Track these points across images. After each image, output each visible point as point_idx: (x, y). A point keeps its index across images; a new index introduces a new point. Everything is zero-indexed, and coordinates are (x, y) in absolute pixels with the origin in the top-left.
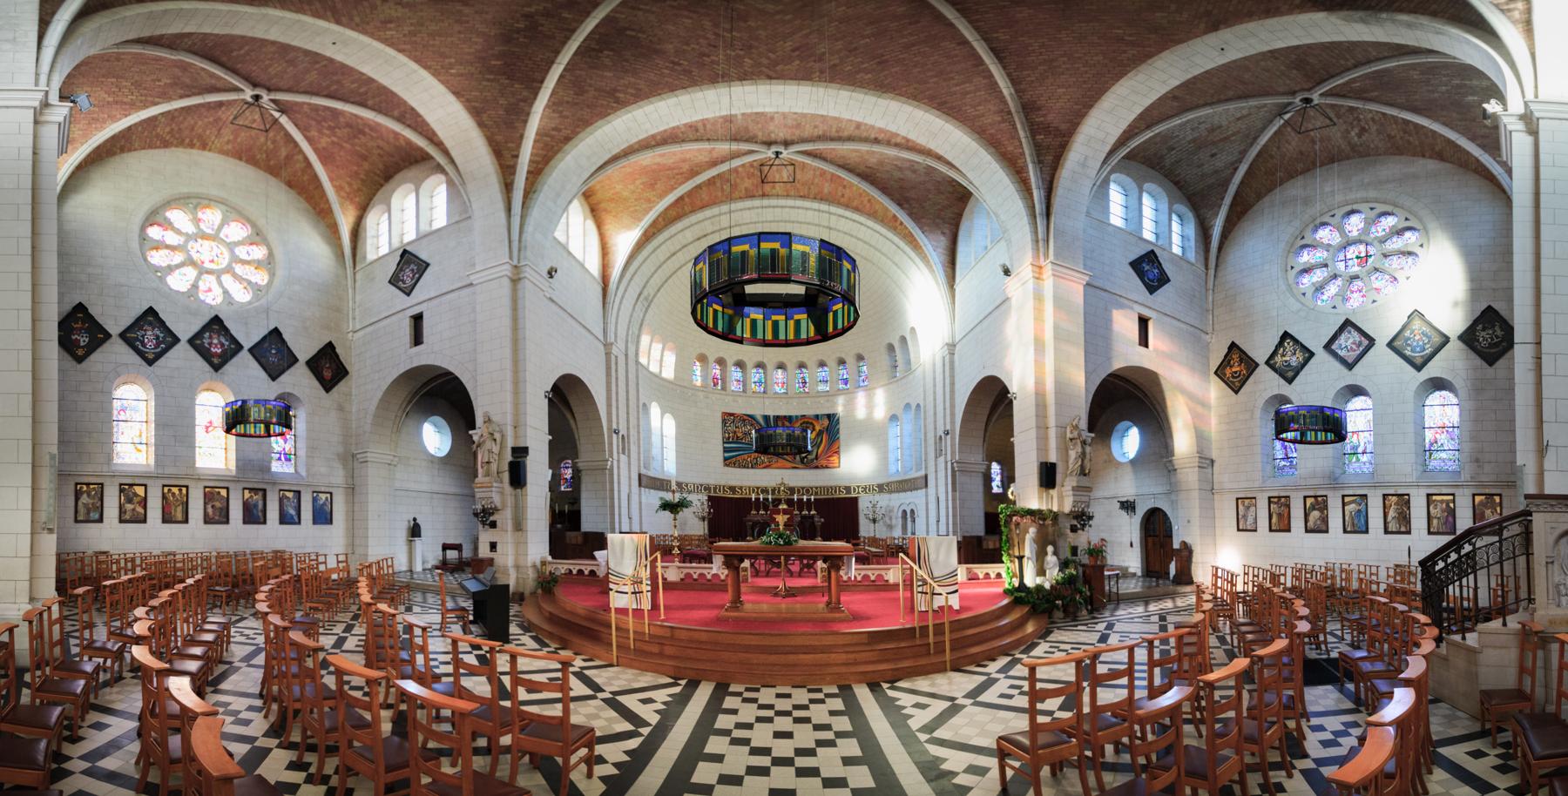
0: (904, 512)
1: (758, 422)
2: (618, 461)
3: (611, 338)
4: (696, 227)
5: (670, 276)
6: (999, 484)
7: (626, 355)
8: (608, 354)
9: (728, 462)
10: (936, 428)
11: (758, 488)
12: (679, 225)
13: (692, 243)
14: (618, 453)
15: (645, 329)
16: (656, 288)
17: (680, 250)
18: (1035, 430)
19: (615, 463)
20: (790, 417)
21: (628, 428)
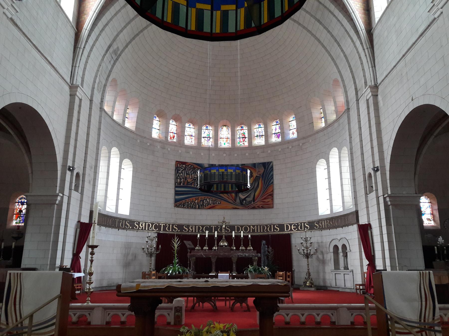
0: (336, 247)
2: (69, 197)
3: (78, 81)
6: (430, 217)
7: (91, 101)
8: (72, 96)
9: (178, 203)
10: (364, 167)
11: (203, 226)
14: (70, 189)
19: (65, 199)
21: (84, 168)
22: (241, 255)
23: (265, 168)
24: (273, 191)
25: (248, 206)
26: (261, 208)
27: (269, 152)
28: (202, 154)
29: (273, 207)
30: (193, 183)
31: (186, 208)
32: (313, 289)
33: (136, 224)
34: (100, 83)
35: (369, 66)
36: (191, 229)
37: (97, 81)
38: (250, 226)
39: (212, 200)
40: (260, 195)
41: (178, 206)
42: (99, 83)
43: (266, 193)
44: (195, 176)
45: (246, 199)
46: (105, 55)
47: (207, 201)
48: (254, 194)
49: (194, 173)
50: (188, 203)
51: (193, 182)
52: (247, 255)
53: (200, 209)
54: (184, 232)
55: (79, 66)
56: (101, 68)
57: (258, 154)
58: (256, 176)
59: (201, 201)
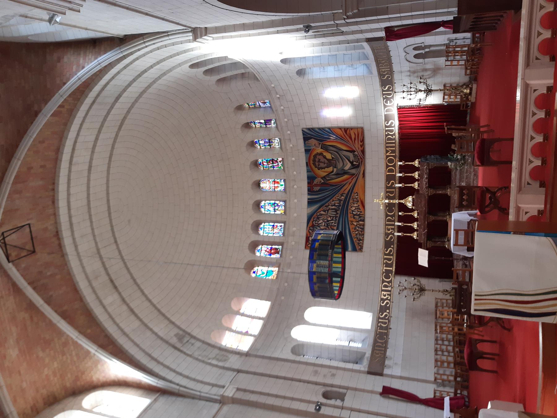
0: (416, 56)
1: (316, 211)
4: (100, 294)
5: (159, 311)
12: (98, 312)
13: (120, 294)
15: (213, 339)
16: (171, 326)
17: (128, 305)
18: (64, 152)
20: (309, 178)
21: (316, 384)
22: (426, 184)
23: (310, 138)
24: (340, 128)
25: (361, 159)
26: (364, 148)
27: (289, 132)
28: (295, 215)
29: (362, 129)
30: (332, 227)
31: (363, 237)
32: (475, 86)
33: (383, 303)
34: (217, 357)
35: (167, 40)
36: (391, 231)
37: (214, 362)
38: (387, 157)
39: (354, 204)
40: (345, 143)
41: (361, 247)
42: (218, 360)
43: (344, 137)
44: (323, 225)
45: (351, 161)
46: (185, 353)
47: (355, 209)
48: (344, 152)
49: (319, 226)
50: (356, 235)
51: (331, 228)
52: (426, 177)
53: (364, 219)
54: (394, 240)
55: (200, 392)
56: (200, 358)
57: (293, 146)
58: (321, 148)
59: (354, 218)
